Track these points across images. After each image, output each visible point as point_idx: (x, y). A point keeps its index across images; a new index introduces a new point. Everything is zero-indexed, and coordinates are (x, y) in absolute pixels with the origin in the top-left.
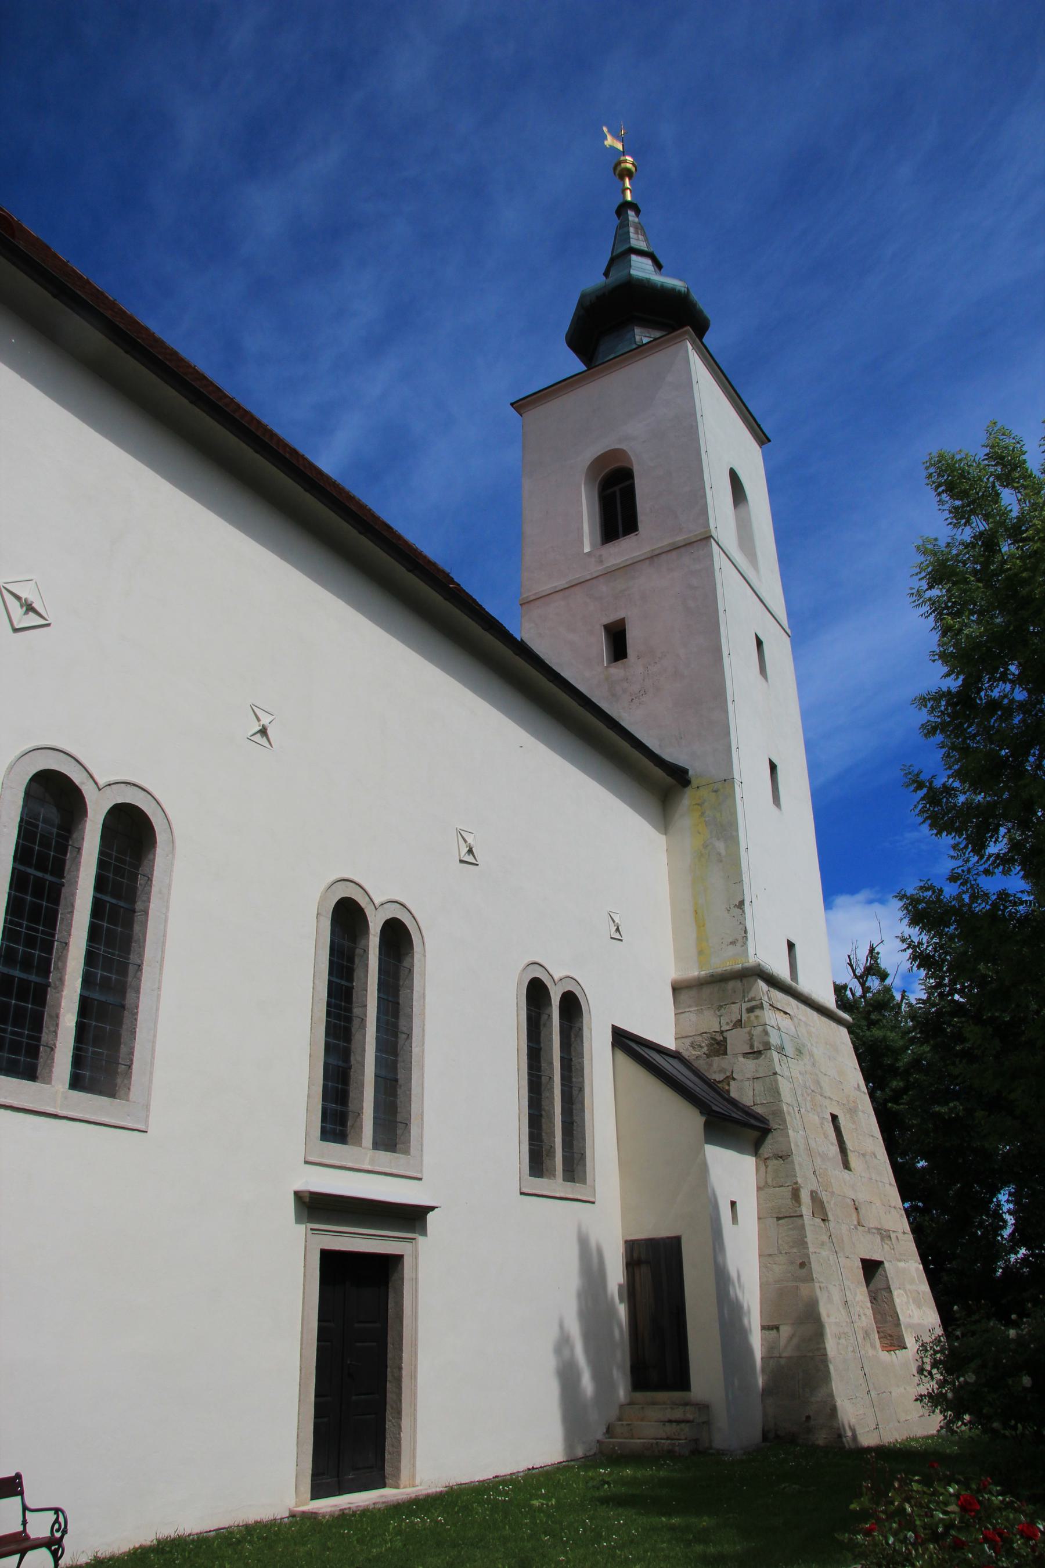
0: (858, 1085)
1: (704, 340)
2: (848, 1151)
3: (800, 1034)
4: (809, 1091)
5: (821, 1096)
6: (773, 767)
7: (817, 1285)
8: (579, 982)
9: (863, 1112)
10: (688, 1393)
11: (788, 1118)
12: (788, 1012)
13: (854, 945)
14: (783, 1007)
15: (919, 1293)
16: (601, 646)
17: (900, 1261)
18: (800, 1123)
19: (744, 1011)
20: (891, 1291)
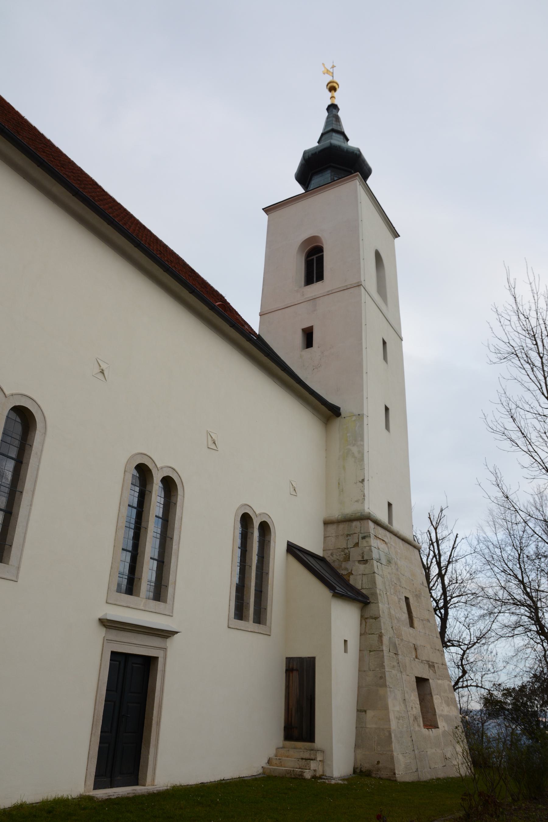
0: (423, 582)
1: (368, 182)
2: (414, 617)
3: (390, 553)
4: (393, 583)
5: (400, 586)
6: (387, 409)
7: (388, 689)
8: (271, 516)
9: (424, 597)
10: (313, 744)
11: (379, 597)
12: (385, 540)
13: (432, 508)
14: (382, 538)
15: (449, 698)
16: (299, 339)
17: (439, 679)
18: (386, 600)
19: (360, 538)
20: (432, 696)
